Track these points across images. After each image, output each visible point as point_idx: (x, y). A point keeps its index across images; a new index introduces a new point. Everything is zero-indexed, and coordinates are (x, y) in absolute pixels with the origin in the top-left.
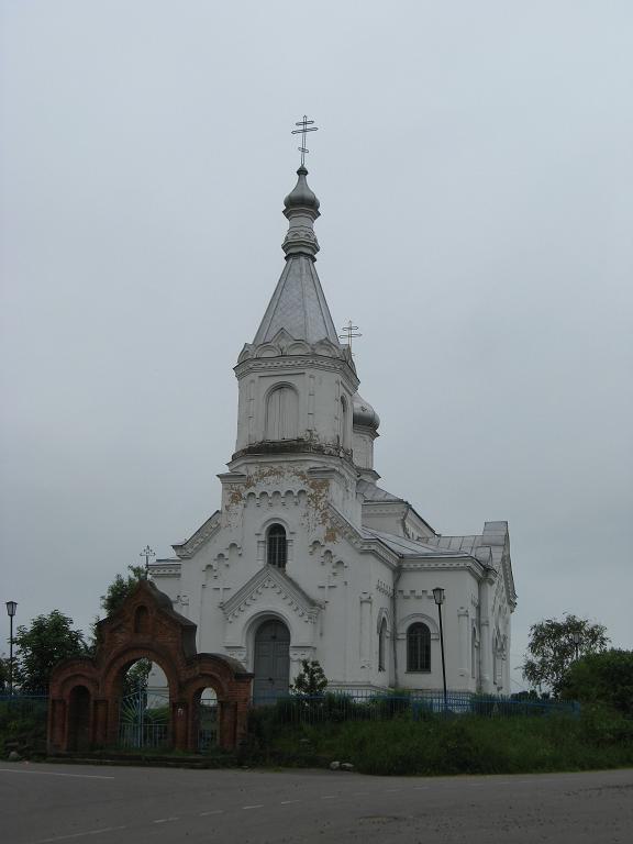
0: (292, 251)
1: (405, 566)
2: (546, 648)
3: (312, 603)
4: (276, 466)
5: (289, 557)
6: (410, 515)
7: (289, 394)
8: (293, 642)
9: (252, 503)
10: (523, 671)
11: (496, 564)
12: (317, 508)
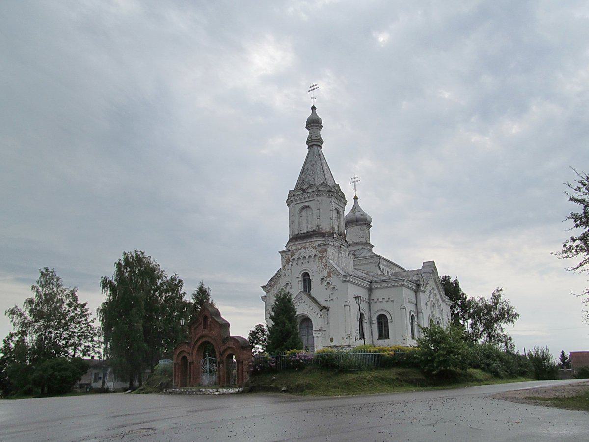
0: (310, 144)
1: (373, 287)
4: (304, 245)
7: (309, 211)
8: (314, 329)
9: (295, 263)
12: (322, 262)
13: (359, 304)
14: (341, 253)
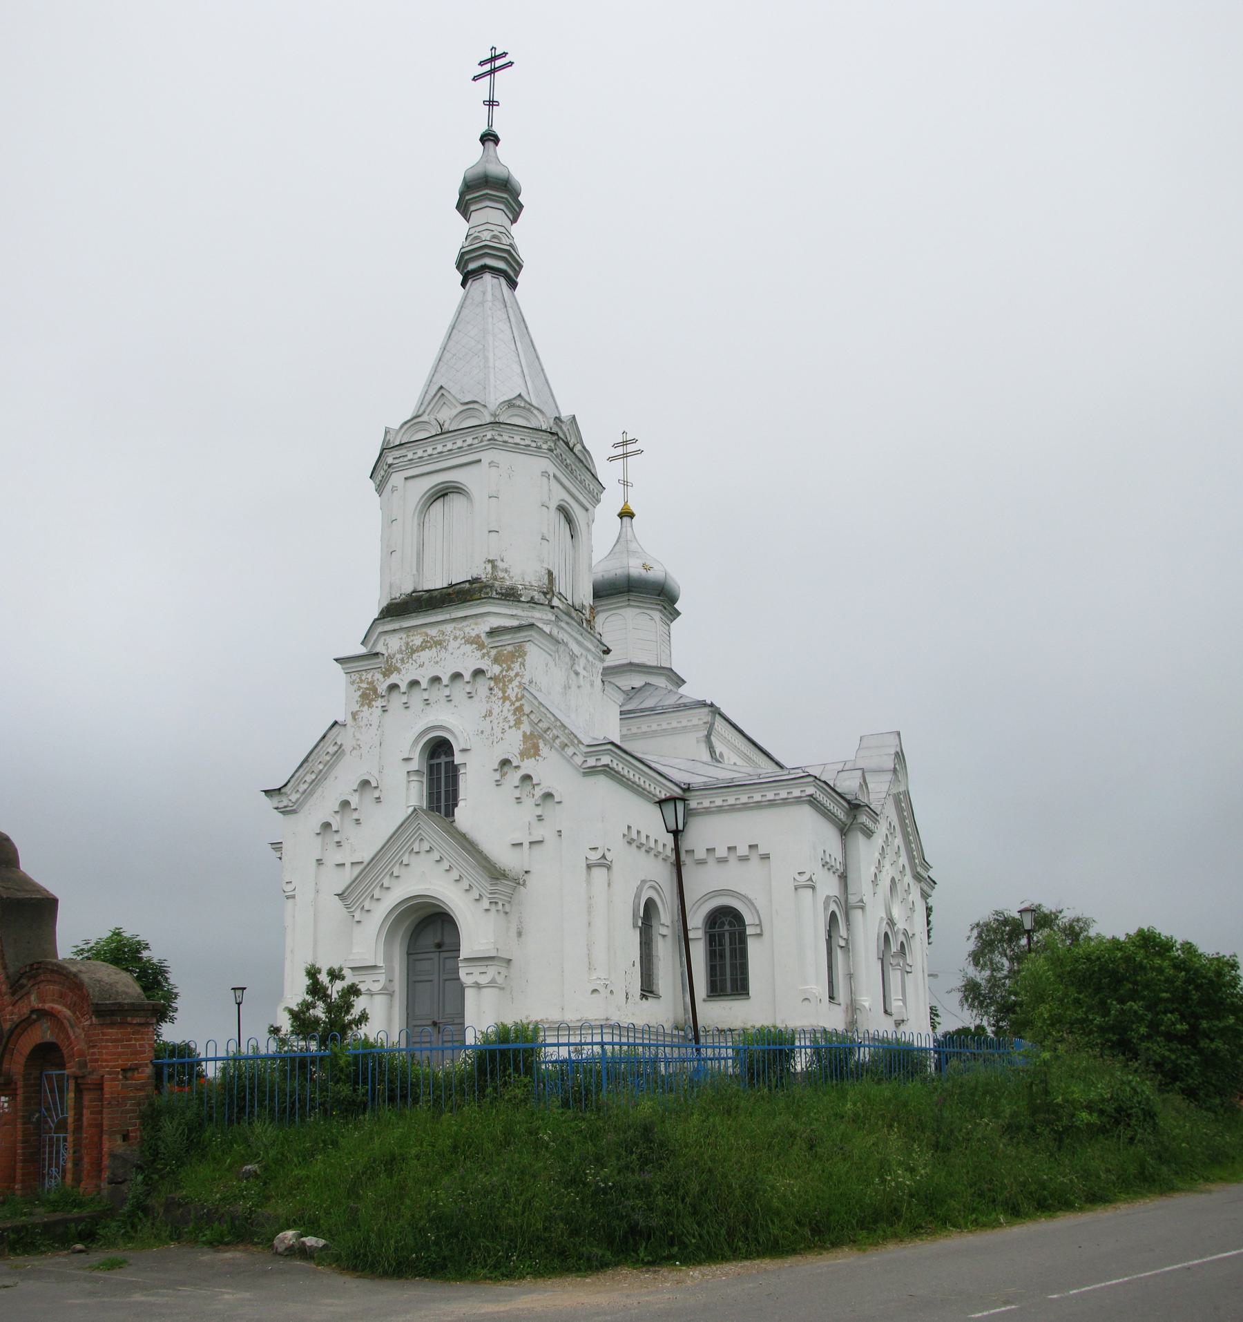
2: (997, 957)
3: (495, 873)
4: (433, 632)
5: (462, 795)
6: (720, 725)
7: (455, 502)
8: (465, 952)
9: (397, 700)
10: (961, 994)
11: (878, 792)
13: (239, 1004)
14: (577, 674)
